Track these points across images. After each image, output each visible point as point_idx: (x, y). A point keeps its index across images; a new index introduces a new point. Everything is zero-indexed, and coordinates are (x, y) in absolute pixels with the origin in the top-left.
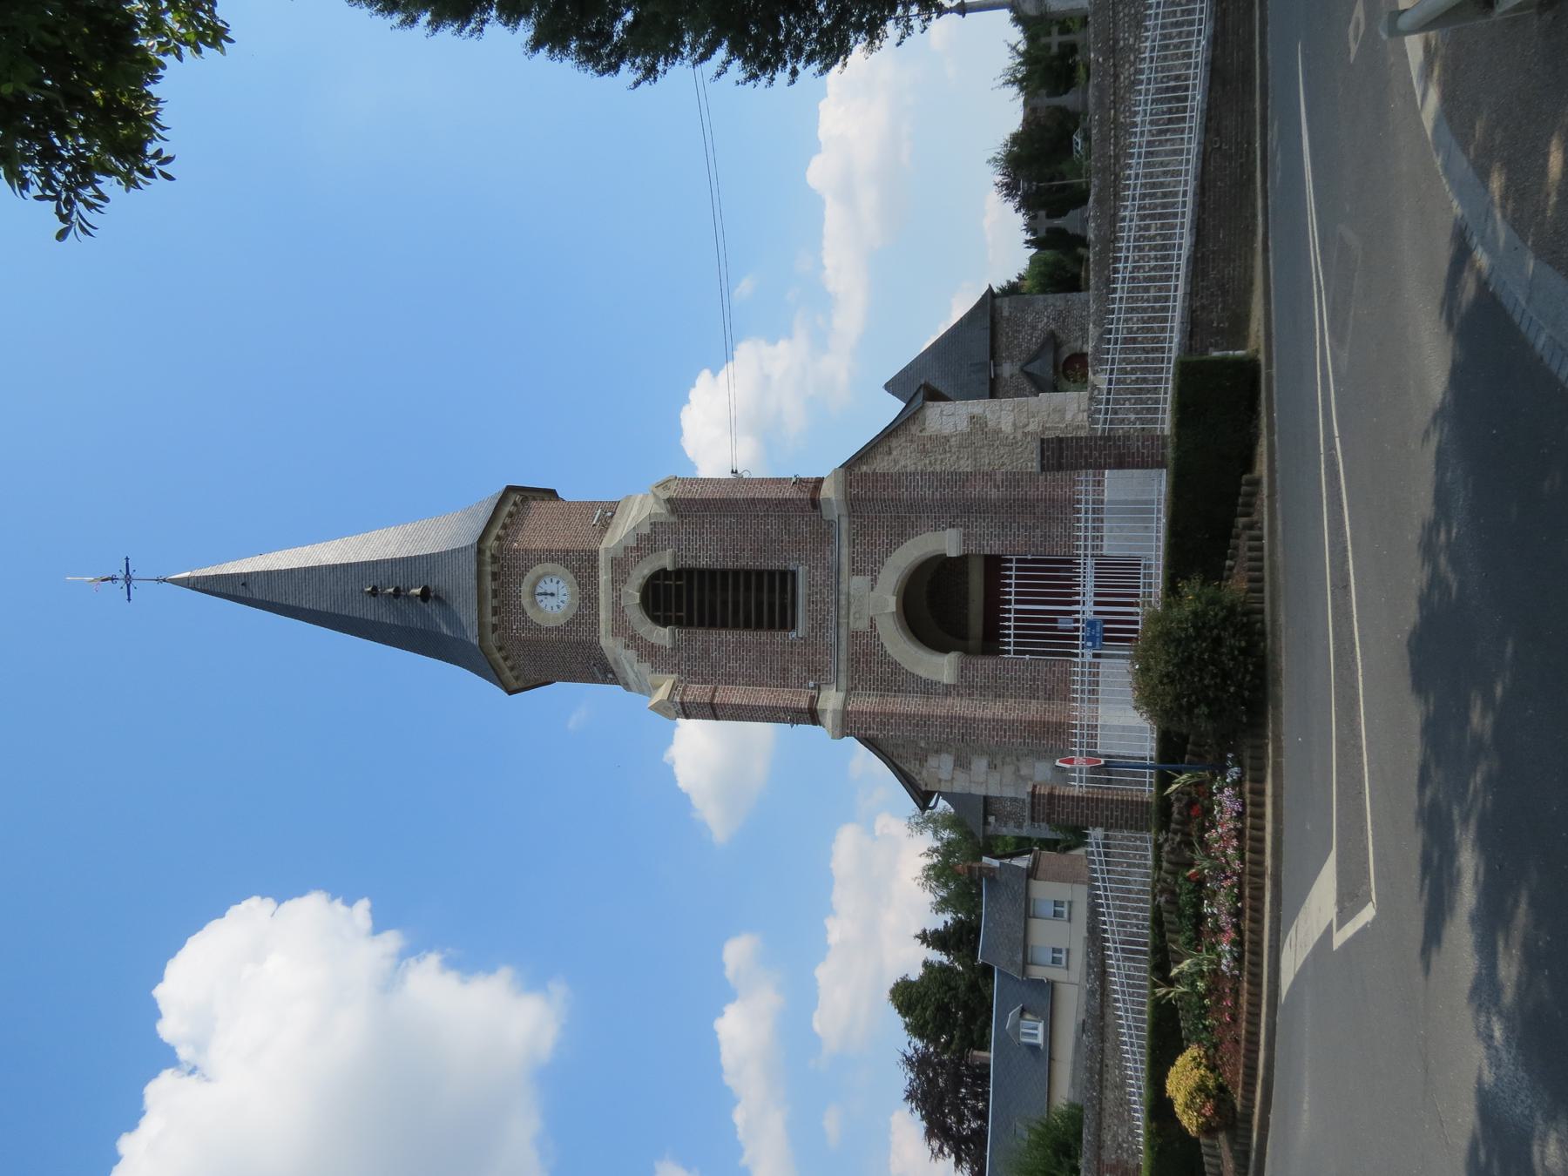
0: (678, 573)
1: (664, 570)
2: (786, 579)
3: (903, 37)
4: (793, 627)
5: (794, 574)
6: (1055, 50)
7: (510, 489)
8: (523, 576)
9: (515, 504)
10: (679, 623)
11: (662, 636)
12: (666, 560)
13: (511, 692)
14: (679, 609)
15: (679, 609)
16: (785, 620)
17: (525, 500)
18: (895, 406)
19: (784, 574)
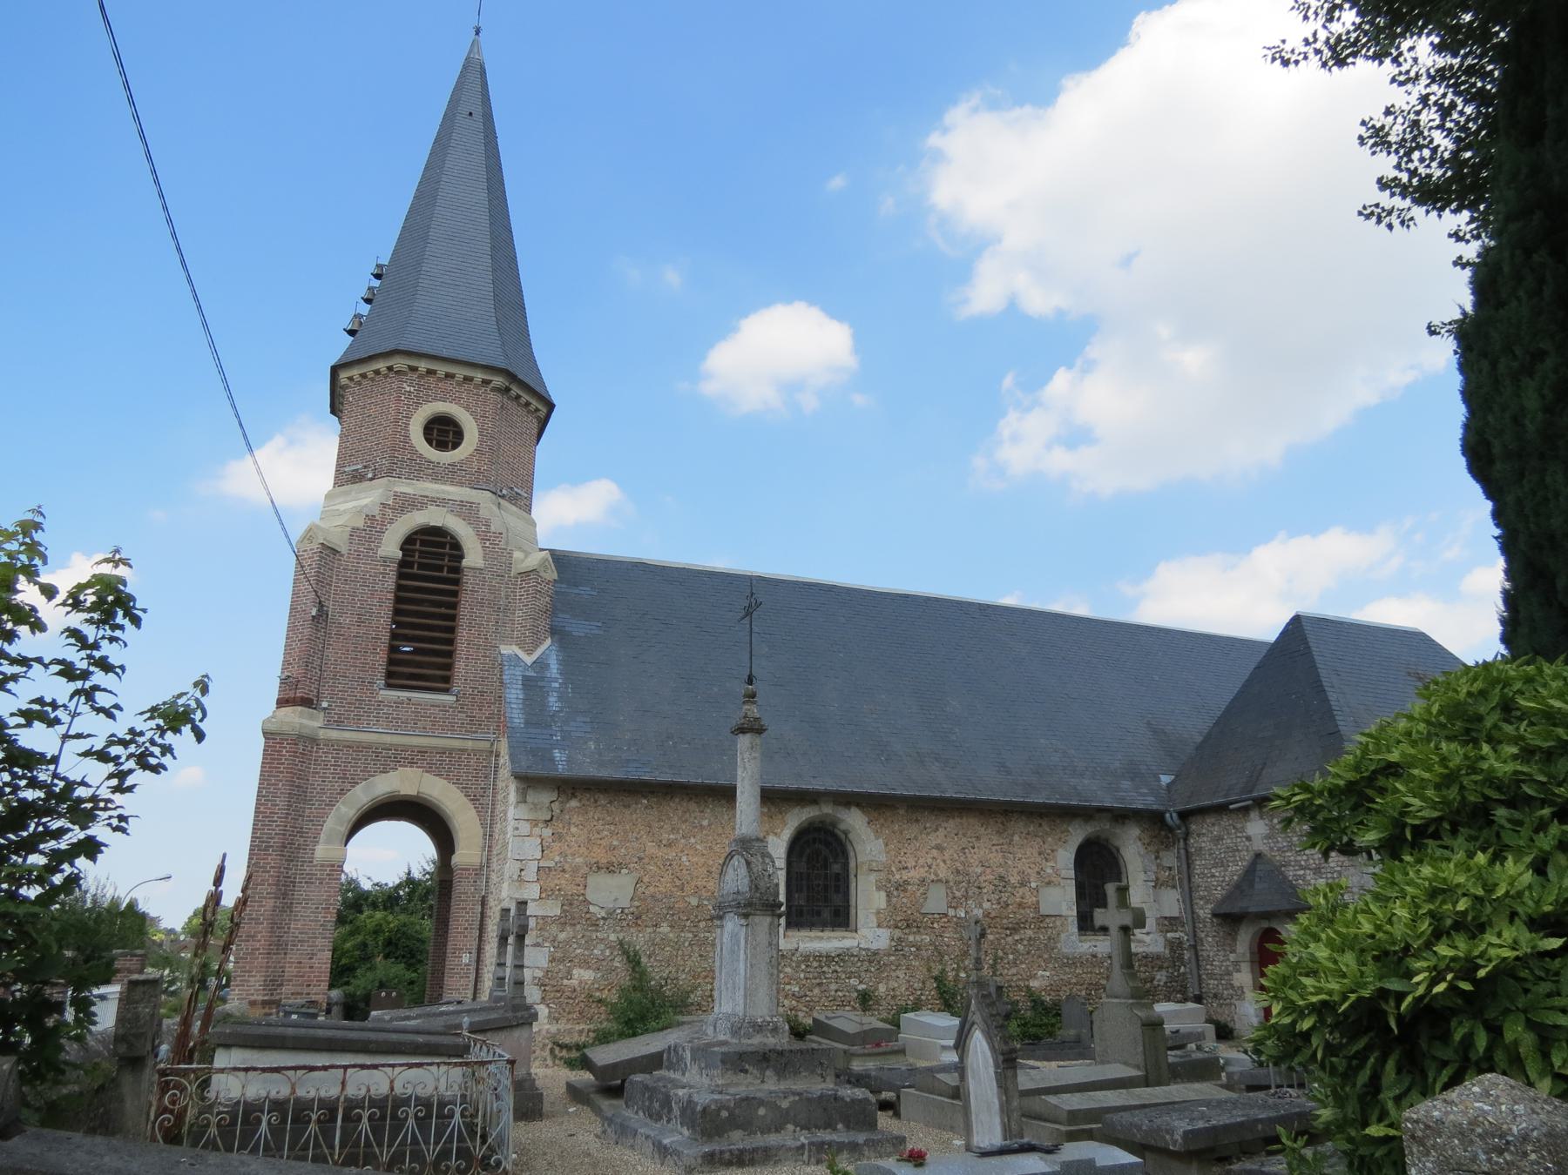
0: (457, 570)
1: (462, 557)
2: (442, 682)
3: (105, 690)
4: (389, 686)
5: (446, 691)
6: (1385, 1007)
7: (551, 407)
8: (467, 408)
9: (537, 410)
10: (403, 564)
11: (391, 547)
12: (473, 557)
13: (335, 370)
14: (422, 566)
15: (422, 566)
16: (394, 678)
17: (538, 418)
18: (36, 724)
19: (447, 680)
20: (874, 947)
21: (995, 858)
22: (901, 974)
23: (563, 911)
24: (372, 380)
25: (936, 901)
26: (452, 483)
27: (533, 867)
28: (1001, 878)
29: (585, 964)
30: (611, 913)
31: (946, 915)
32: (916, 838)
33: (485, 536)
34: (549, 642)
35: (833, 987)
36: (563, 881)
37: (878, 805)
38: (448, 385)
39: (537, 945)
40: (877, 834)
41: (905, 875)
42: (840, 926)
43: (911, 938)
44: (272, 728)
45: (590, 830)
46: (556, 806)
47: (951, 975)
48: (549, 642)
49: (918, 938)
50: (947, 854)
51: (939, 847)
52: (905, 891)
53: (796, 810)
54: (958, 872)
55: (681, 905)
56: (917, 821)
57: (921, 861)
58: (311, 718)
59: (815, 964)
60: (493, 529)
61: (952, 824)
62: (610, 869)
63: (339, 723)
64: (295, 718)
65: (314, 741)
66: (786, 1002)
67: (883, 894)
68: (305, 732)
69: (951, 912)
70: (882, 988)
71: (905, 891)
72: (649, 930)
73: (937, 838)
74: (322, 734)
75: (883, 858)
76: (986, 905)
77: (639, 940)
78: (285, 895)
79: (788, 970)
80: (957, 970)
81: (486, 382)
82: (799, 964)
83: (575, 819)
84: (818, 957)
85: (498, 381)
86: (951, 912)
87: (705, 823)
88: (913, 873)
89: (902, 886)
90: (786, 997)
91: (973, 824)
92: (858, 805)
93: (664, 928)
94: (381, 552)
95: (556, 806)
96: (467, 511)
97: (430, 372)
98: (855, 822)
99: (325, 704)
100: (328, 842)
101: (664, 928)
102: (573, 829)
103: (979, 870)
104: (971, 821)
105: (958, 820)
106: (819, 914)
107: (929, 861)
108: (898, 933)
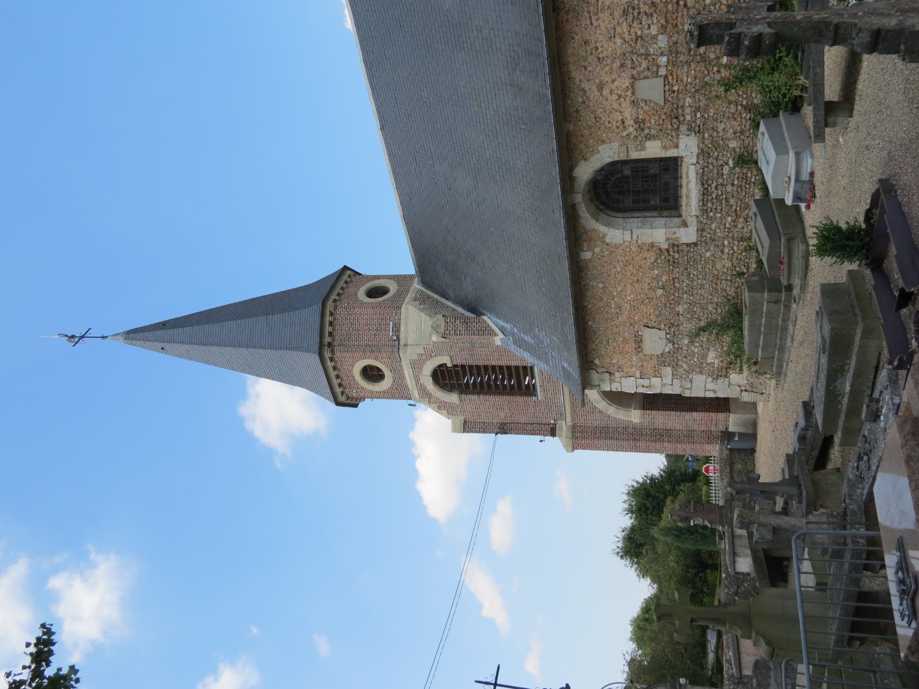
12: (446, 360)
20: (695, 150)
21: (604, 21)
22: (721, 127)
23: (669, 365)
24: (335, 319)
25: (652, 90)
26: (402, 370)
27: (640, 381)
28: (625, 13)
29: (705, 356)
30: (669, 341)
31: (666, 77)
32: (594, 112)
33: (429, 355)
34: (485, 318)
35: (729, 188)
36: (649, 367)
37: (568, 152)
38: (343, 375)
39: (691, 382)
40: (595, 152)
41: (630, 122)
42: (677, 165)
43: (688, 118)
44: (571, 448)
45: (613, 350)
46: (600, 370)
47: (724, 73)
48: (485, 318)
49: (688, 110)
50: (607, 79)
51: (601, 87)
52: (644, 121)
53: (583, 222)
54: (622, 66)
55: (663, 299)
56: (577, 111)
57: (615, 106)
58: (561, 428)
59: (710, 205)
60: (423, 352)
61: (577, 75)
62: (639, 341)
63: (562, 416)
64: (564, 426)
65: (574, 427)
66: (740, 226)
67: (648, 144)
68: (570, 435)
69: (662, 71)
70: (733, 144)
71: (644, 121)
72: (681, 318)
73: (591, 88)
74: (570, 423)
75: (615, 145)
76: (654, 30)
77: (687, 326)
78: (661, 435)
79: (713, 226)
80: (720, 65)
81: (332, 359)
82: (708, 218)
83: (607, 360)
84: (703, 202)
85: (327, 355)
86: (662, 71)
87: (601, 285)
88: (627, 114)
89: (640, 123)
90: (735, 226)
91: (573, 48)
92: (571, 169)
93: (680, 309)
94: (458, 402)
95: (600, 370)
96: (417, 365)
97: (340, 385)
98: (585, 172)
99: (552, 422)
100: (630, 417)
101: (680, 309)
102: (614, 361)
103: (619, 41)
104: (570, 51)
105: (572, 67)
106: (666, 184)
107: (614, 97)
108: (683, 128)
